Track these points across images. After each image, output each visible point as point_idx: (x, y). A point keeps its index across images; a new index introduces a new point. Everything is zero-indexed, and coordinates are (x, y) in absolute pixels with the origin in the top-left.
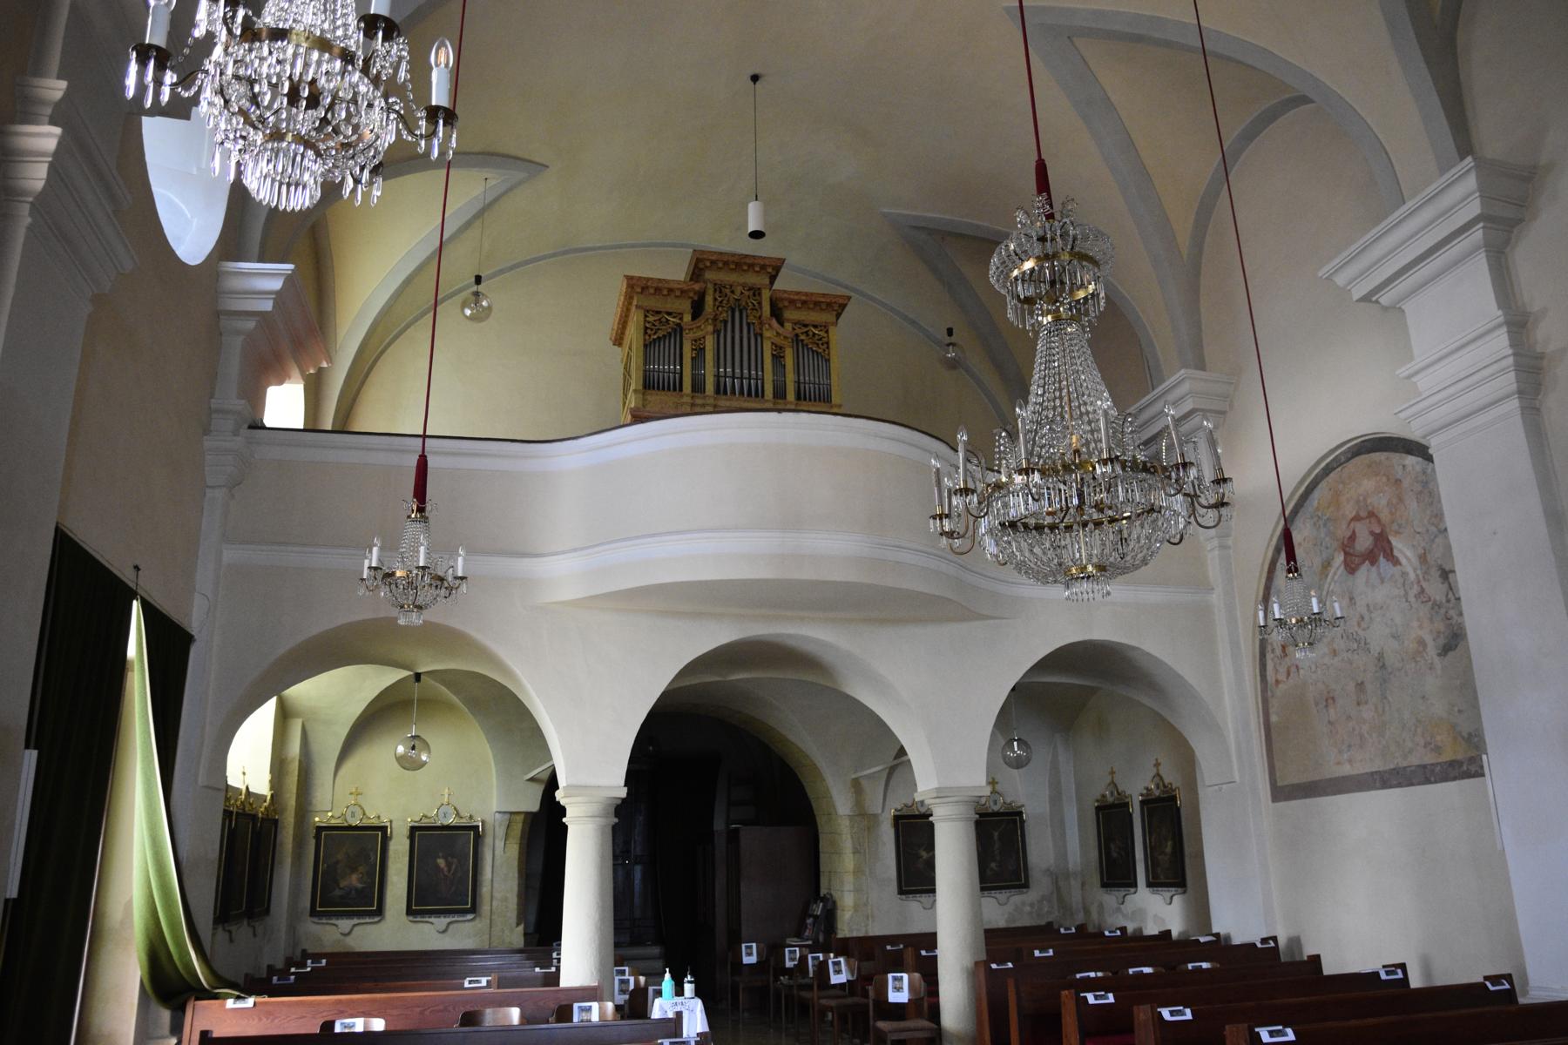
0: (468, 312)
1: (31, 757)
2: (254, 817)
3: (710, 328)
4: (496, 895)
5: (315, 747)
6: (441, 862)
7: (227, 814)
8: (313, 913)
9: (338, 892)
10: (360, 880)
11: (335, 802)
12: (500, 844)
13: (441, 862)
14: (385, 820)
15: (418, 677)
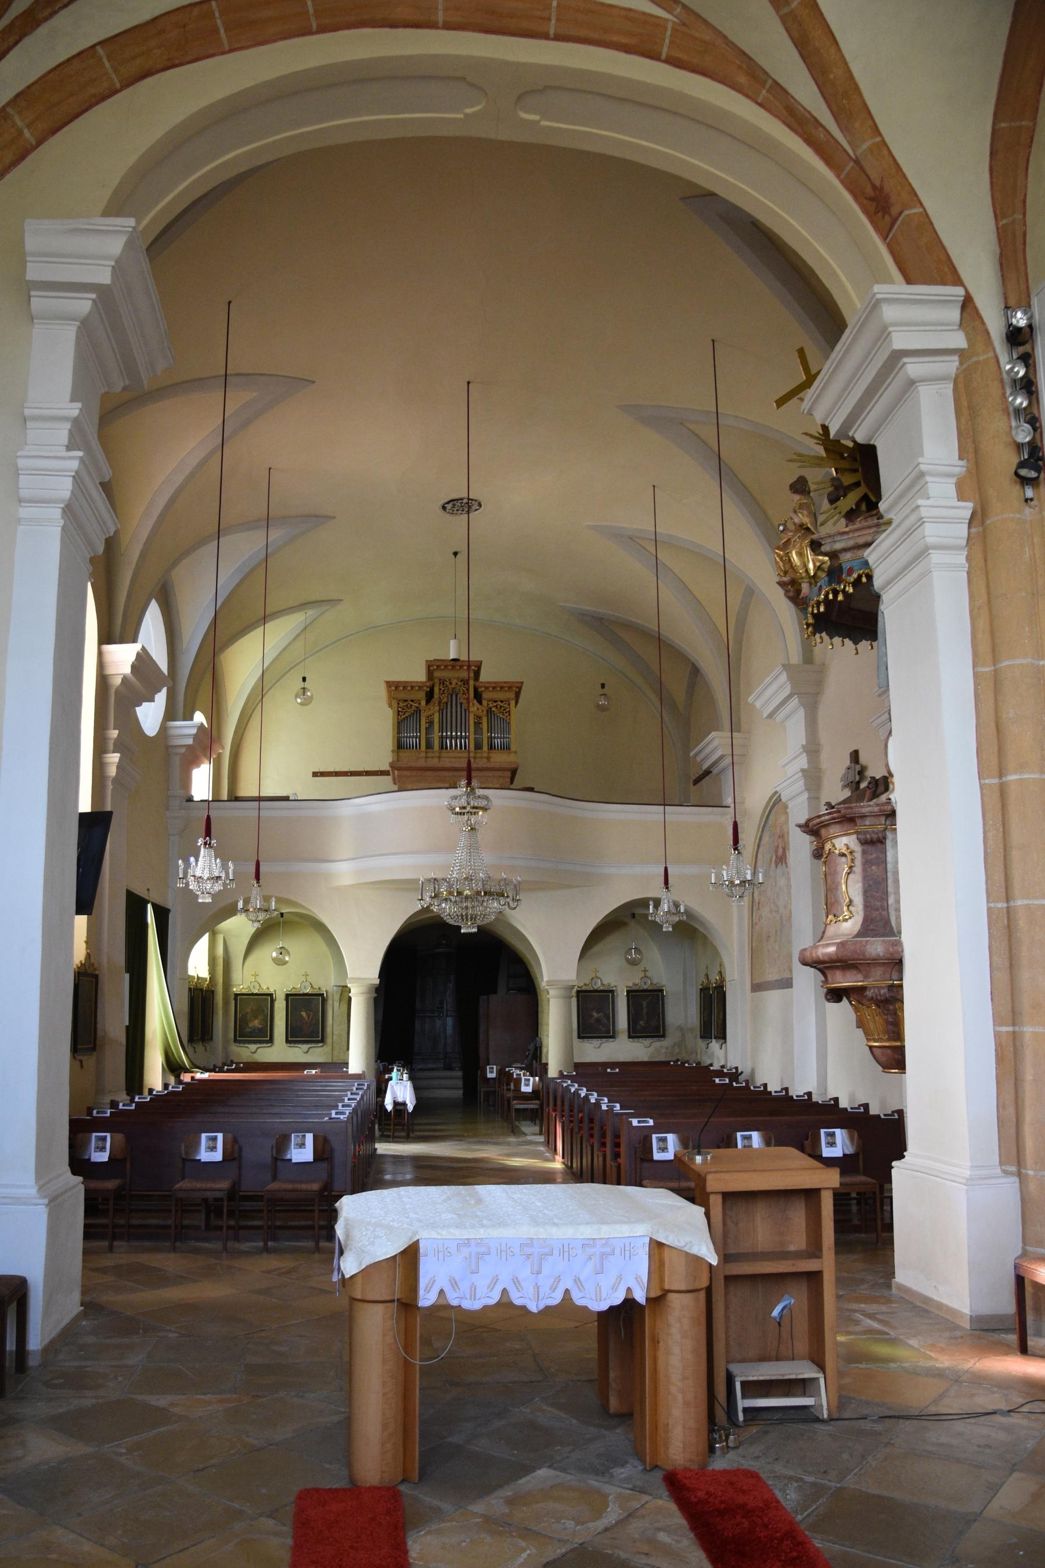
0: (299, 701)
1: (127, 976)
2: (202, 990)
3: (437, 708)
4: (335, 1032)
5: (231, 949)
6: (304, 1014)
7: (190, 989)
8: (235, 1041)
9: (248, 1030)
10: (260, 1023)
11: (243, 981)
12: (336, 1004)
13: (304, 1014)
14: (272, 991)
15: (282, 915)
